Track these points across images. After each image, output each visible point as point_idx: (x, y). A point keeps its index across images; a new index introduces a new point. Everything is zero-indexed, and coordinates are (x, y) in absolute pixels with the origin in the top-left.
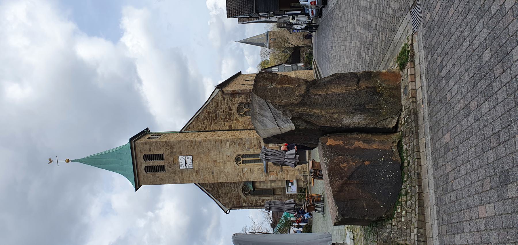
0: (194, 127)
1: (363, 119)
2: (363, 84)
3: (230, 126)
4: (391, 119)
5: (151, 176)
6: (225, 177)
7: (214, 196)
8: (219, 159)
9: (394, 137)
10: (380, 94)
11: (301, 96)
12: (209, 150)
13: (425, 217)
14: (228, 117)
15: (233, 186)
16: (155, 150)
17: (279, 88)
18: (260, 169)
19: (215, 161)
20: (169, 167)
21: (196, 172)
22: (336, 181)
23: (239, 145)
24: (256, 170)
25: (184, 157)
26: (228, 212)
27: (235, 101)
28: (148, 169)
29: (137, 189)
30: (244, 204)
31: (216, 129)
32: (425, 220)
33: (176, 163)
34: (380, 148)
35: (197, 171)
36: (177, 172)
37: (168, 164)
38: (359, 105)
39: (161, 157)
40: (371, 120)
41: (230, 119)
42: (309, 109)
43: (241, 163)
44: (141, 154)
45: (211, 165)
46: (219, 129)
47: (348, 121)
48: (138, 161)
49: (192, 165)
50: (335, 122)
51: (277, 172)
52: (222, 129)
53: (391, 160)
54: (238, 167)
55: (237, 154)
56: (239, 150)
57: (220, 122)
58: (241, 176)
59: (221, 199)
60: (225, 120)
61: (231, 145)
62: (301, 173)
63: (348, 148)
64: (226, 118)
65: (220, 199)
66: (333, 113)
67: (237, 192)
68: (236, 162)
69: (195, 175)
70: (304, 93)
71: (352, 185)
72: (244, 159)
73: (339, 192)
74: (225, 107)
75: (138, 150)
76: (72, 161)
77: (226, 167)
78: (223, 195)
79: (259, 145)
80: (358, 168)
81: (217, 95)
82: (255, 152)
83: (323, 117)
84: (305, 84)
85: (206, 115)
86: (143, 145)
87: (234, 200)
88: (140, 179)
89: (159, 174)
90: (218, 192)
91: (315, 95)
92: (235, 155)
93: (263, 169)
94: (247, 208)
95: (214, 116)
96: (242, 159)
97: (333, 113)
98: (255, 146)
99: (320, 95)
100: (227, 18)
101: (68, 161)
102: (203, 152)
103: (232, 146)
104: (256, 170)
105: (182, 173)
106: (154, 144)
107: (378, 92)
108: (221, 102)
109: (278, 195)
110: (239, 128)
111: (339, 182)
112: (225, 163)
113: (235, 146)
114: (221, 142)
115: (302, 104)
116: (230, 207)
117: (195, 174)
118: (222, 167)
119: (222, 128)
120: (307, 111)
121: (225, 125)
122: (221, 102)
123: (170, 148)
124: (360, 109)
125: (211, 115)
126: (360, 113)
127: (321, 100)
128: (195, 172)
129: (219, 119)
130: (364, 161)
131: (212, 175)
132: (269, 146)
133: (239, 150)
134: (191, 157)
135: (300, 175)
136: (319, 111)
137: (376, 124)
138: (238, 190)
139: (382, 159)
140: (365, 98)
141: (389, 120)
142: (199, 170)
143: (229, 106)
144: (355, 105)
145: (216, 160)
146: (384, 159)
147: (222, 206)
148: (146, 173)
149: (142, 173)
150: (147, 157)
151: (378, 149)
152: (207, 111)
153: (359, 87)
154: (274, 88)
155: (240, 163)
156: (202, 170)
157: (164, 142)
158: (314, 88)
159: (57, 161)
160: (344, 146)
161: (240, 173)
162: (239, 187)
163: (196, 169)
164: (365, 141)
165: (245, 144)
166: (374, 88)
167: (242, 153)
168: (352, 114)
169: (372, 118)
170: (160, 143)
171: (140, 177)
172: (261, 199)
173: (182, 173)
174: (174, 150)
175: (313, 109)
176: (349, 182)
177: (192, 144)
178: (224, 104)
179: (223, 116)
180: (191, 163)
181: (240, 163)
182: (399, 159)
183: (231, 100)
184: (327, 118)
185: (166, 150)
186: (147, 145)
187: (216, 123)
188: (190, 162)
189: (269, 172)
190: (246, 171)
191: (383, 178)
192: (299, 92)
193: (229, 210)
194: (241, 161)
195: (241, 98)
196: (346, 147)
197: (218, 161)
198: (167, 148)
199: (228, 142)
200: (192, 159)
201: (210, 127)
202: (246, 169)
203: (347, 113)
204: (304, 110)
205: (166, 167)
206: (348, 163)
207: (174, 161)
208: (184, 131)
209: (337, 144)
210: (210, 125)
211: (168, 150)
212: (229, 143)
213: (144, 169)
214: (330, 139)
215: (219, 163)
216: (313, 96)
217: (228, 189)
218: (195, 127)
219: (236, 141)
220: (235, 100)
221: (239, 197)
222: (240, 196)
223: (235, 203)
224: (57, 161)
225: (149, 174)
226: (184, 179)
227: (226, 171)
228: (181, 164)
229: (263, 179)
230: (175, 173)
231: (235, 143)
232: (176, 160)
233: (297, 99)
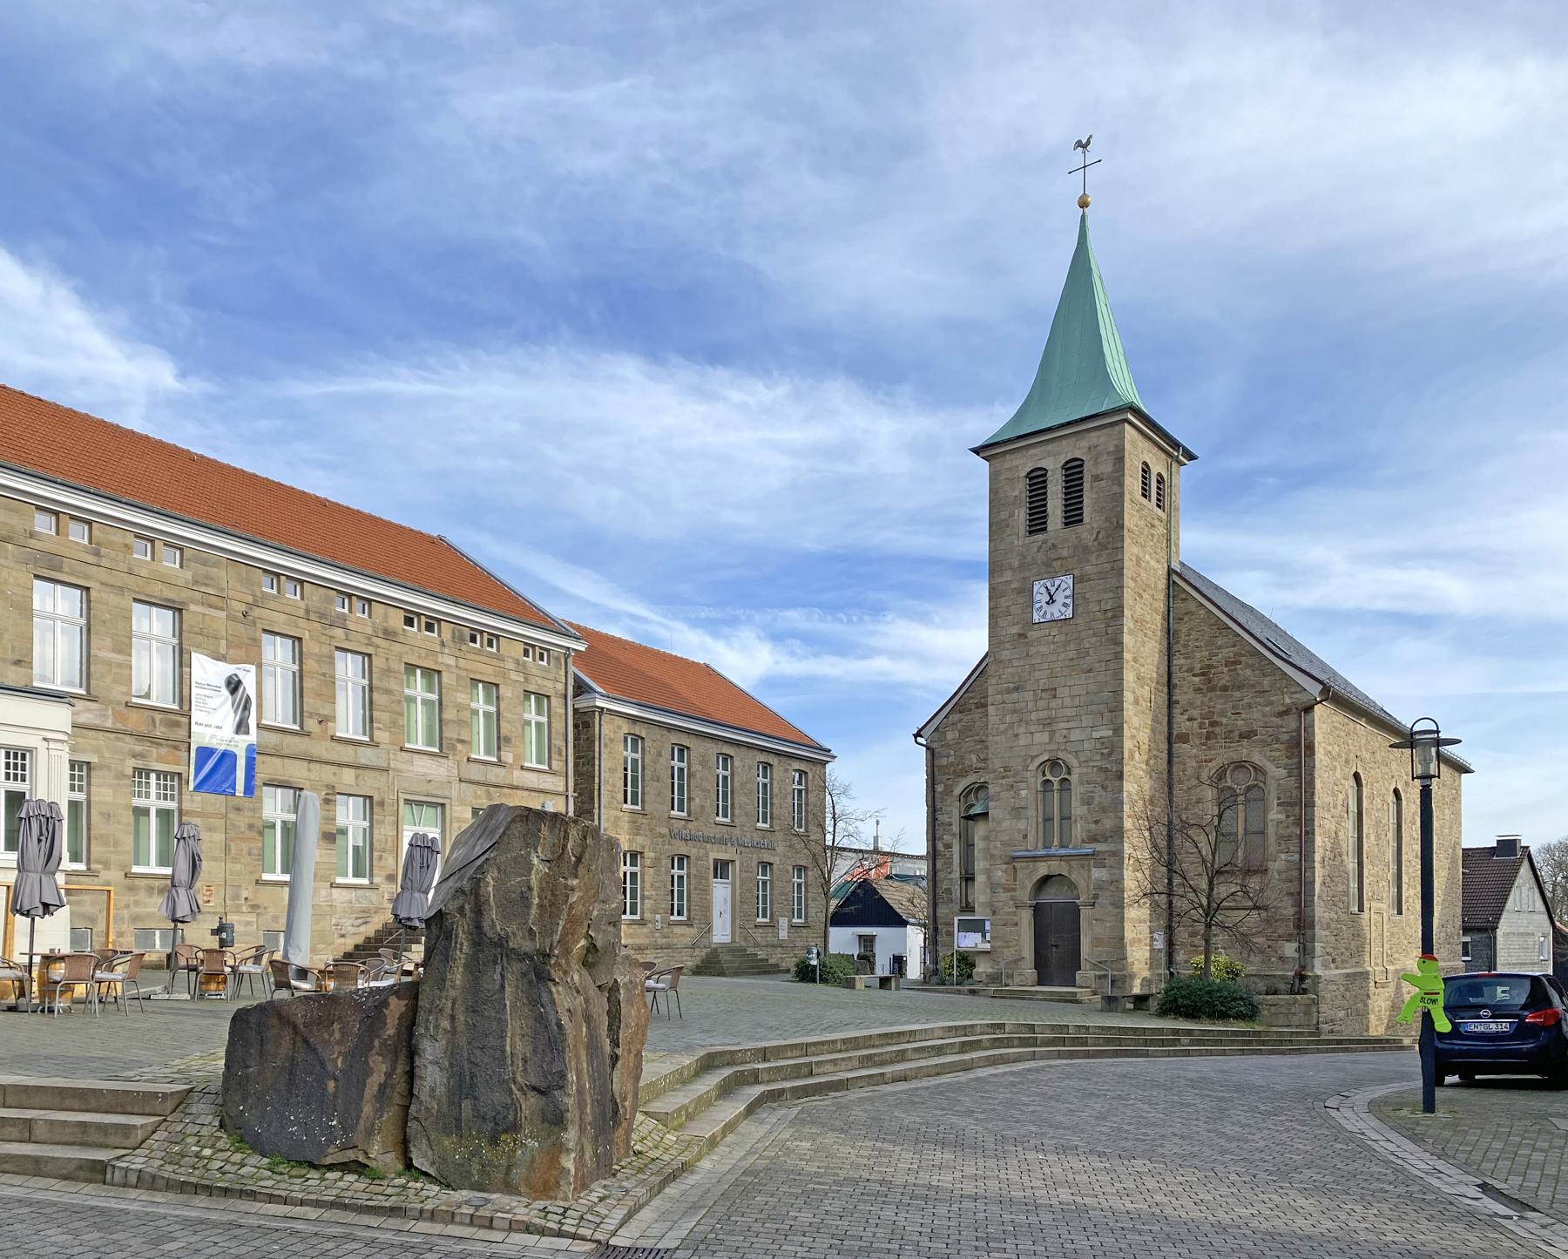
0: (1186, 614)
1: (433, 1090)
2: (529, 1105)
3: (1184, 738)
4: (431, 1158)
5: (1016, 493)
6: (1003, 727)
8: (1057, 705)
9: (391, 1161)
10: (494, 1141)
11: (501, 938)
12: (1090, 671)
13: (161, 1190)
16: (1097, 493)
17: (529, 881)
18: (1025, 836)
19: (1053, 692)
20: (1041, 547)
21: (1020, 635)
22: (306, 1010)
24: (1022, 825)
26: (919, 739)
27: (1273, 754)
28: (1037, 479)
29: (976, 451)
30: (940, 788)
31: (1177, 691)
32: (155, 1190)
34: (362, 1122)
35: (1026, 637)
36: (1027, 574)
37: (1049, 543)
38: (473, 1086)
39: (1073, 516)
40: (427, 1108)
41: (1208, 738)
42: (463, 956)
45: (1041, 682)
46: (1178, 702)
47: (431, 1051)
48: (1064, 442)
49: (1042, 620)
50: (427, 1020)
51: (1014, 890)
52: (1177, 711)
53: (330, 1142)
54: (1033, 767)
55: (1073, 762)
56: (1085, 770)
57: (1199, 703)
58: (1004, 777)
59: (955, 717)
60: (1207, 721)
63: (374, 1047)
66: (453, 1018)
68: (1048, 760)
69: (1014, 632)
70: (511, 945)
71: (291, 1046)
72: (1056, 786)
73: (280, 1016)
74: (1255, 717)
75: (1099, 437)
76: (1083, 217)
77: (1033, 728)
79: (1099, 837)
80: (323, 1065)
81: (1300, 689)
82: (1076, 821)
83: (441, 991)
84: (538, 951)
85: (1227, 653)
88: (1008, 457)
89: (1021, 516)
90: (977, 708)
91: (502, 976)
92: (1070, 756)
93: (1024, 848)
94: (930, 799)
96: (1055, 780)
97: (453, 1018)
98: (1096, 822)
99: (503, 987)
102: (1082, 653)
103: (1098, 746)
104: (1022, 825)
105: (1020, 591)
107: (503, 1137)
108: (1271, 703)
109: (964, 890)
110: (1175, 769)
111: (302, 1016)
112: (1047, 724)
113: (1098, 757)
114: (1111, 711)
115: (479, 937)
116: (934, 745)
117: (1015, 630)
118: (1033, 716)
119: (1180, 711)
120: (458, 953)
121: (1189, 720)
122: (1271, 703)
124: (463, 1085)
125: (1225, 670)
126: (449, 1083)
127: (489, 991)
128: (1021, 632)
129: (1210, 700)
130: (336, 1080)
132: (1094, 869)
133: (1085, 770)
135: (1003, 963)
136: (458, 982)
137: (416, 1119)
139: (334, 1123)
140: (490, 1102)
141: (430, 1153)
142: (1027, 643)
144: (472, 1076)
145: (1055, 697)
146: (333, 1126)
148: (1025, 474)
149: (1024, 464)
150: (1073, 472)
151: (358, 1117)
152: (1241, 655)
153: (521, 1089)
154: (530, 867)
155: (1044, 775)
157: (1121, 522)
158: (524, 975)
160: (379, 1037)
161: (1015, 775)
164: (383, 1088)
166: (515, 1127)
167: (1074, 778)
168: (447, 1063)
169: (433, 1111)
170: (1119, 509)
171: (1013, 457)
173: (1020, 591)
174: (1093, 558)
175: (465, 966)
176: (299, 1039)
177: (1110, 614)
178: (1264, 715)
179: (1223, 713)
180: (1048, 617)
181: (1044, 775)
182: (328, 1160)
183: (1278, 741)
184: (438, 1002)
185: (1096, 531)
186: (1115, 464)
187: (1198, 690)
190: (1019, 794)
191: (292, 1118)
192: (514, 934)
193: (925, 743)
194: (1049, 777)
195: (1283, 772)
196: (376, 1043)
197: (1054, 703)
198: (1103, 533)
200: (1063, 617)
201: (1185, 668)
202: (1023, 793)
203: (453, 1052)
204: (462, 944)
205: (1040, 537)
206: (339, 1043)
207: (1059, 562)
208: (1174, 582)
209: (388, 1021)
210: (1190, 670)
211: (1094, 536)
214: (406, 1005)
216: (498, 968)
218: (1186, 619)
219: (1113, 758)
220: (1279, 752)
221: (963, 774)
223: (944, 761)
224: (1085, 167)
227: (1022, 730)
229: (996, 847)
230: (1023, 567)
231: (1110, 754)
232: (1062, 566)
233: (493, 926)
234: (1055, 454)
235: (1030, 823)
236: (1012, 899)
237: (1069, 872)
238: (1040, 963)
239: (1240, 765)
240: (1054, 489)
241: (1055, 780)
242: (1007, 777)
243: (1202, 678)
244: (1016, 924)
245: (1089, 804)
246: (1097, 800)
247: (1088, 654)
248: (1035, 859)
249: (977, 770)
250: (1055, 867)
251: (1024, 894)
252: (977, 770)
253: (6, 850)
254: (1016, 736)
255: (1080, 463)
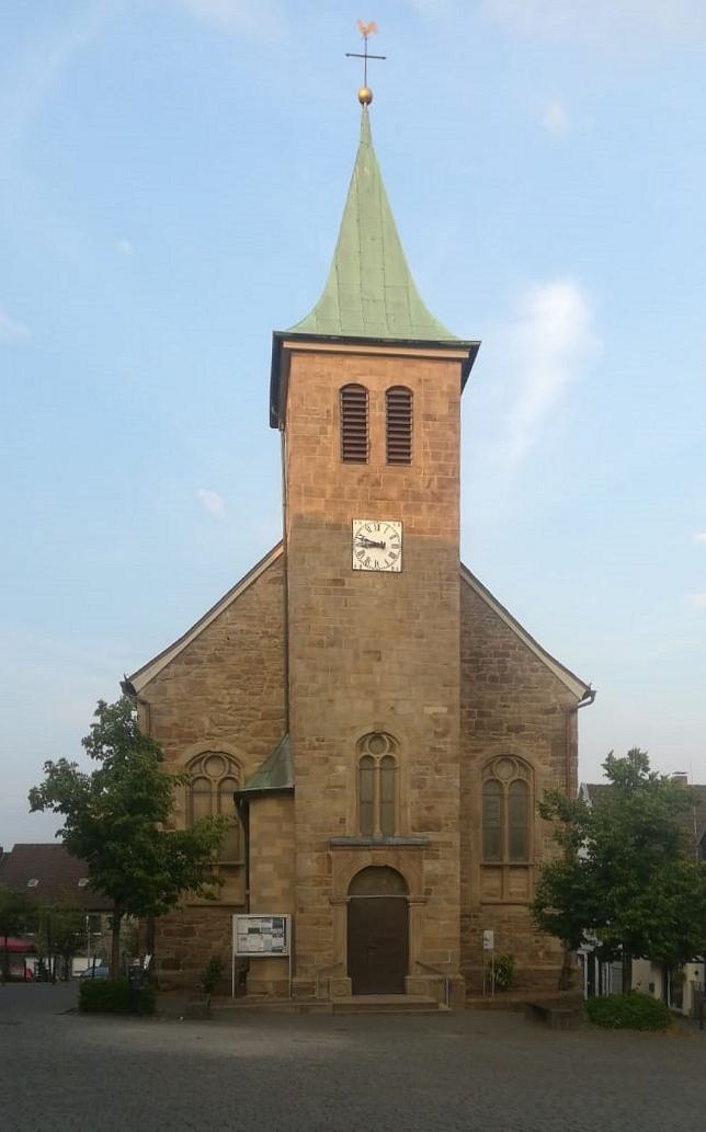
7: (195, 643)
14: (485, 720)
15: (231, 718)
18: (343, 821)
19: (377, 656)
21: (336, 581)
23: (433, 749)
24: (338, 807)
25: (359, 549)
33: (376, 508)
39: (399, 451)
43: (364, 754)
44: (416, 380)
49: (364, 568)
54: (354, 739)
58: (314, 748)
59: (182, 668)
61: (436, 721)
62: (321, 972)
64: (481, 714)
65: (180, 664)
67: (206, 731)
78: (198, 679)
86: (449, 394)
87: (175, 719)
90: (210, 661)
92: (398, 731)
95: (493, 673)
100: (33, 810)
101: (366, 101)
106: (450, 433)
112: (370, 692)
114: (445, 686)
117: (329, 574)
123: (433, 493)
131: (324, 638)
134: (397, 566)
138: (214, 735)
143: (522, 728)
145: (379, 659)
147: (154, 671)
156: (346, 606)
159: (368, 54)
162: (226, 741)
163: (347, 580)
165: (438, 771)
172: (178, 820)
177: (444, 577)
180: (372, 564)
183: (544, 737)
188: (377, 563)
189: (328, 855)
197: (377, 667)
199: (445, 710)
200: (390, 569)
202: (341, 769)
205: (360, 467)
212: (441, 714)
213: (358, 382)
215: (370, 671)
217: (220, 699)
221: (191, 739)
222: (192, 742)
225: (333, 402)
226: (314, 531)
228: (372, 527)
234: (382, 375)
235: (346, 806)
236: (326, 893)
237: (398, 864)
238: (355, 967)
239: (215, 756)
240: (377, 414)
241: (378, 757)
242: (320, 748)
243: (471, 665)
244: (331, 924)
245: (419, 787)
246: (429, 783)
247: (418, 617)
248: (357, 847)
249: (210, 736)
250: (385, 858)
251: (341, 889)
252: (210, 736)
253: (274, 332)
254: (331, 701)
255: (407, 394)
